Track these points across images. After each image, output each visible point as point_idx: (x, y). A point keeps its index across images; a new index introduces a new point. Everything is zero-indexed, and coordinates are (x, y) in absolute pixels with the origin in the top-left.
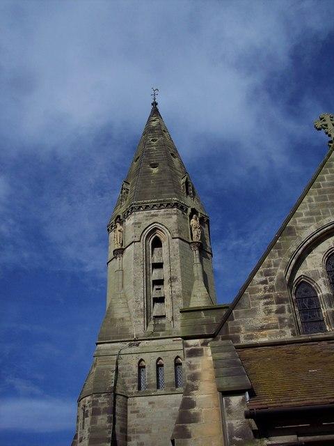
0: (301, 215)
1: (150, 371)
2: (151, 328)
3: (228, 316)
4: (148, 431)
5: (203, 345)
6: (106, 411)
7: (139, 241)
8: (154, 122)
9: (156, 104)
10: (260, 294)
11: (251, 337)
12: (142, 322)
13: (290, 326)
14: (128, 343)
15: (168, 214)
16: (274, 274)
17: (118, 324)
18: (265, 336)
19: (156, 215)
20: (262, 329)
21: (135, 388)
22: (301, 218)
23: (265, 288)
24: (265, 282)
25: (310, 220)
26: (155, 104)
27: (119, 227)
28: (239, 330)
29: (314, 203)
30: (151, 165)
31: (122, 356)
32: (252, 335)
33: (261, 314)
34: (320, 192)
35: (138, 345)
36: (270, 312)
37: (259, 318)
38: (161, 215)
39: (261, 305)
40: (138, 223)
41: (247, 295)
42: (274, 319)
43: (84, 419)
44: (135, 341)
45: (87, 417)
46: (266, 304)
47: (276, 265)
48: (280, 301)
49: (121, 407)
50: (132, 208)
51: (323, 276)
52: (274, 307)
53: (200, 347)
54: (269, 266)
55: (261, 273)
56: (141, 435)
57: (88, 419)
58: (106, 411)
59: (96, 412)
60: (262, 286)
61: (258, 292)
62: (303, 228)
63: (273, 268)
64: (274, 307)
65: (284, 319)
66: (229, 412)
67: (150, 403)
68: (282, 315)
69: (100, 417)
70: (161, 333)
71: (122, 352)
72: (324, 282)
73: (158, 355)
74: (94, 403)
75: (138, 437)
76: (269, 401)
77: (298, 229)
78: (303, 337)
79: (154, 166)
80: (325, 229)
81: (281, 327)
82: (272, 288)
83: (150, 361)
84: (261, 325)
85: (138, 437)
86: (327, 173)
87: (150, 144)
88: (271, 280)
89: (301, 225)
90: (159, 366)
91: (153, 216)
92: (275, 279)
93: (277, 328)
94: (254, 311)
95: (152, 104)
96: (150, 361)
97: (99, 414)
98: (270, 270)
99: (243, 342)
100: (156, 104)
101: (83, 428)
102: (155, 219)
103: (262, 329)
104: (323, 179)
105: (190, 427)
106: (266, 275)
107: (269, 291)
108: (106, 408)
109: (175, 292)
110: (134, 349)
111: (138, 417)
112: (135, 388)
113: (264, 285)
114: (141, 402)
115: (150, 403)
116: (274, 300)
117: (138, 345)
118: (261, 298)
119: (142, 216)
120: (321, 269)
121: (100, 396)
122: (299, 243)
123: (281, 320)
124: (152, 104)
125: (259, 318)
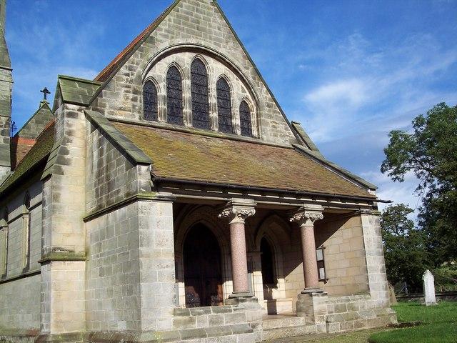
10: (123, 83)
13: (139, 112)
16: (135, 71)
20: (121, 109)
22: (161, 32)
24: (127, 75)
28: (105, 106)
32: (113, 112)
33: (121, 99)
36: (127, 98)
52: (131, 96)
53: (76, 112)
60: (125, 77)
64: (131, 96)
66: (140, 174)
68: (135, 103)
82: (131, 81)
94: (117, 95)
103: (121, 109)
120: (164, 76)
122: (156, 52)
123: (134, 106)
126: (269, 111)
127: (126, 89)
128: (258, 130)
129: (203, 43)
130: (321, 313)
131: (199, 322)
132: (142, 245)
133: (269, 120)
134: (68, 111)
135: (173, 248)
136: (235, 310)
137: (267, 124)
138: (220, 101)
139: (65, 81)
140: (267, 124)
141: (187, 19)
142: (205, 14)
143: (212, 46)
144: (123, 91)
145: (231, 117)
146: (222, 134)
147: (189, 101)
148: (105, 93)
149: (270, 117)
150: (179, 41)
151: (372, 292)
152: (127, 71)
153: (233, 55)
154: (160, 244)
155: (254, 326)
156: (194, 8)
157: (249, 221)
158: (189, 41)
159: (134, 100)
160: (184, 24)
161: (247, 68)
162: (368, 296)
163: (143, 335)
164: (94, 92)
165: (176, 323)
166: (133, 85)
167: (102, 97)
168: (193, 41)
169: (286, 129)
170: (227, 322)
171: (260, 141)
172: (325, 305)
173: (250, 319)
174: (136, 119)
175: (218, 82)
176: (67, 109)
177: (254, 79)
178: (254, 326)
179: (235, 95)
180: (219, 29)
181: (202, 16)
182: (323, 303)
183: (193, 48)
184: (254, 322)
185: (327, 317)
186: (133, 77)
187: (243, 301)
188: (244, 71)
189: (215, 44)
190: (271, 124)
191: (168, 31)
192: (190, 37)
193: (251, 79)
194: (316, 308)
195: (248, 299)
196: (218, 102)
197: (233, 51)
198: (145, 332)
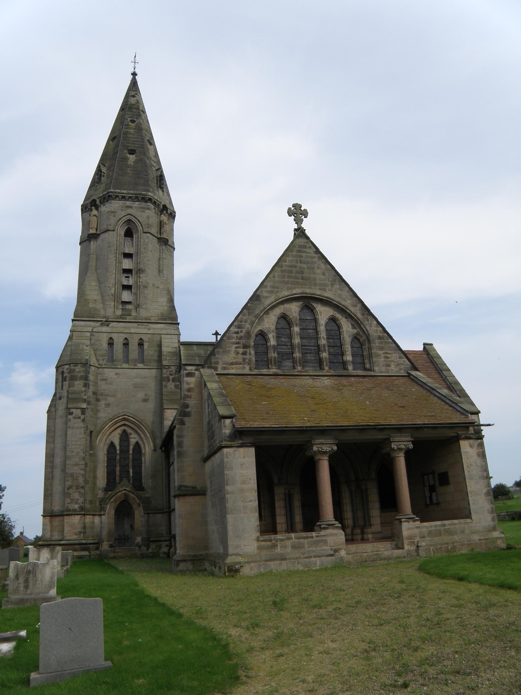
0: (266, 287)
1: (118, 347)
2: (119, 312)
3: (212, 353)
4: (114, 396)
5: (195, 370)
6: (81, 378)
7: (113, 231)
8: (132, 99)
9: (136, 75)
10: (234, 340)
11: (225, 368)
12: (112, 306)
13: (249, 364)
14: (100, 323)
15: (141, 208)
16: (243, 328)
17: (91, 305)
18: (233, 369)
19: (131, 207)
20: (232, 364)
21: (105, 361)
22: (266, 289)
23: (237, 337)
24: (237, 333)
25: (271, 292)
26: (134, 74)
27: (95, 212)
28: (217, 363)
29: (276, 279)
30: (129, 150)
31: (94, 333)
32: (226, 367)
33: (232, 354)
34: (282, 271)
35: (108, 325)
36: (238, 353)
37: (231, 357)
38: (136, 207)
39: (233, 348)
40: (114, 212)
41: (225, 340)
42: (240, 358)
43: (62, 382)
44: (107, 322)
45: (66, 381)
46: (236, 347)
47: (246, 322)
48: (245, 346)
49: (93, 375)
50: (109, 196)
51: (273, 332)
52: (241, 350)
53: (193, 371)
54: (241, 322)
55: (236, 326)
56: (108, 398)
57: (66, 383)
58: (81, 378)
59: (73, 378)
60: (235, 335)
61: (232, 339)
62: (267, 297)
63: (243, 323)
64: (241, 350)
65: (246, 359)
66: (225, 426)
67: (116, 374)
68: (245, 357)
69: (77, 383)
70: (128, 317)
71: (95, 330)
72: (273, 336)
73: (124, 336)
74: (71, 371)
75: (106, 399)
76: (241, 424)
77: (263, 297)
78: (255, 372)
79: (132, 152)
80: (280, 300)
81: (244, 364)
82: (241, 338)
83: (119, 340)
84: (231, 361)
85: (106, 399)
86: (289, 256)
87: (128, 125)
88: (241, 332)
89: (265, 294)
90: (126, 344)
91: (128, 207)
92: (244, 331)
93: (241, 364)
94: (229, 352)
95: (132, 74)
96: (119, 340)
97: (76, 380)
98: (241, 325)
99: (220, 371)
100: (136, 75)
101: (62, 389)
102: (129, 211)
103: (232, 364)
104: (285, 261)
105: (186, 419)
106: (239, 328)
107: (239, 339)
108: (82, 376)
109: (142, 282)
110: (104, 329)
111: (106, 384)
112: (105, 361)
113: (237, 335)
114: (110, 373)
115: (116, 374)
116: (241, 346)
117: (108, 325)
118: (233, 343)
119: (117, 205)
120: (273, 327)
121: (77, 366)
122: (262, 308)
123: (244, 360)
124: (132, 74)
125: (231, 357)
126: (381, 343)
127: (236, 345)
128: (370, 363)
129: (308, 291)
130: (411, 537)
131: (281, 547)
132: (227, 485)
133: (381, 352)
134: (187, 372)
135: (255, 486)
136: (317, 536)
137: (378, 356)
138: (331, 340)
139: (185, 346)
140: (378, 356)
141: (291, 272)
142: (308, 263)
143: (317, 292)
144: (233, 348)
145: (343, 354)
146: (332, 373)
147: (298, 346)
148: (218, 352)
149: (382, 348)
150: (285, 293)
151: (474, 516)
152: (236, 330)
153: (340, 296)
154: (244, 482)
155: (336, 551)
156: (297, 260)
157: (408, 454)
158: (294, 292)
159: (244, 353)
160: (288, 277)
161: (355, 306)
162: (469, 520)
163: (229, 558)
164: (209, 352)
165: (259, 548)
166: (243, 341)
167: (215, 355)
168: (297, 291)
169: (400, 358)
170: (309, 547)
171: (373, 374)
172: (416, 531)
173: (333, 545)
174: (247, 371)
175: (326, 323)
176: (186, 370)
177: (363, 314)
178: (336, 551)
179: (345, 333)
180: (324, 274)
181: (305, 266)
182: (413, 528)
183: (298, 297)
184: (336, 547)
185: (418, 542)
186: (242, 334)
187: (325, 528)
188: (352, 309)
189: (320, 289)
190: (383, 356)
191: (273, 287)
192: (295, 288)
193: (359, 316)
194: (405, 533)
195: (330, 527)
196: (328, 342)
197: (339, 292)
198: (231, 555)
